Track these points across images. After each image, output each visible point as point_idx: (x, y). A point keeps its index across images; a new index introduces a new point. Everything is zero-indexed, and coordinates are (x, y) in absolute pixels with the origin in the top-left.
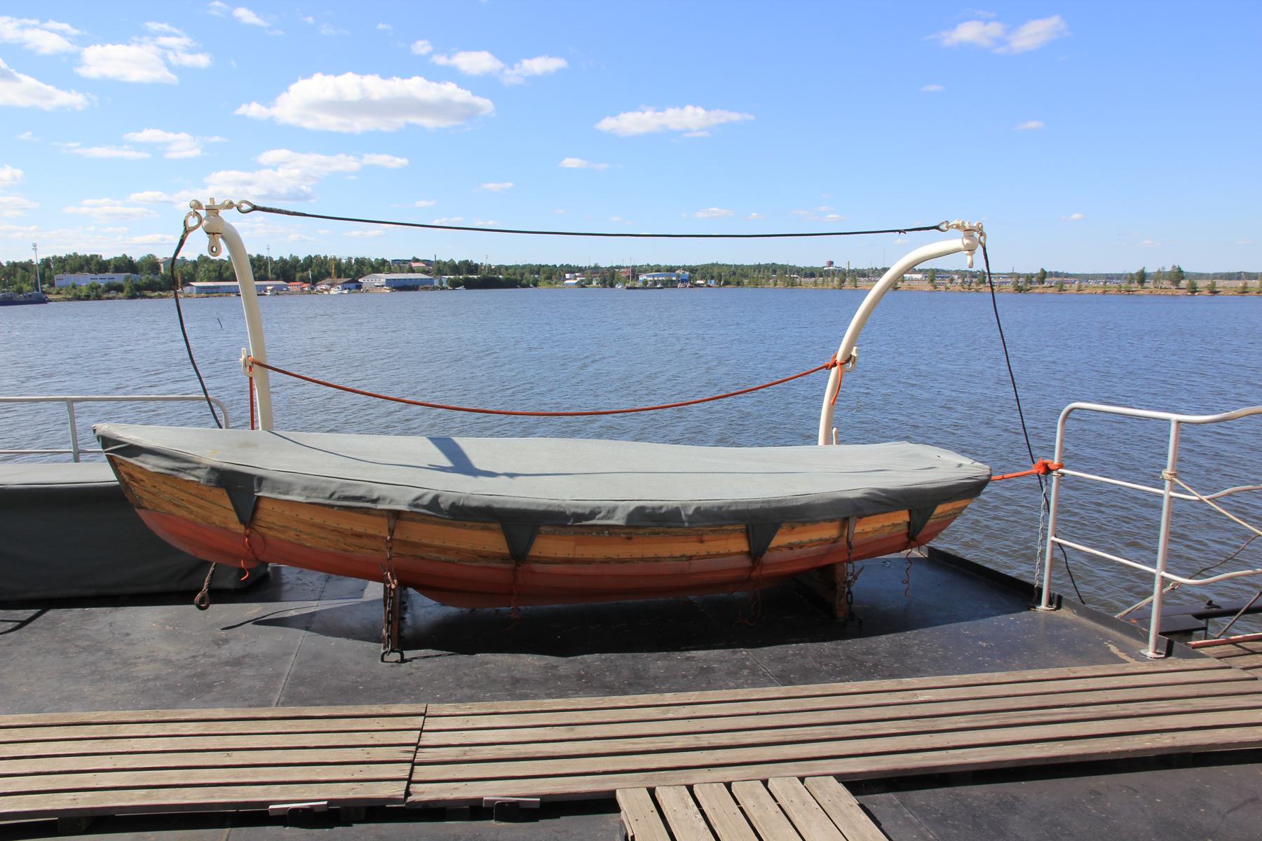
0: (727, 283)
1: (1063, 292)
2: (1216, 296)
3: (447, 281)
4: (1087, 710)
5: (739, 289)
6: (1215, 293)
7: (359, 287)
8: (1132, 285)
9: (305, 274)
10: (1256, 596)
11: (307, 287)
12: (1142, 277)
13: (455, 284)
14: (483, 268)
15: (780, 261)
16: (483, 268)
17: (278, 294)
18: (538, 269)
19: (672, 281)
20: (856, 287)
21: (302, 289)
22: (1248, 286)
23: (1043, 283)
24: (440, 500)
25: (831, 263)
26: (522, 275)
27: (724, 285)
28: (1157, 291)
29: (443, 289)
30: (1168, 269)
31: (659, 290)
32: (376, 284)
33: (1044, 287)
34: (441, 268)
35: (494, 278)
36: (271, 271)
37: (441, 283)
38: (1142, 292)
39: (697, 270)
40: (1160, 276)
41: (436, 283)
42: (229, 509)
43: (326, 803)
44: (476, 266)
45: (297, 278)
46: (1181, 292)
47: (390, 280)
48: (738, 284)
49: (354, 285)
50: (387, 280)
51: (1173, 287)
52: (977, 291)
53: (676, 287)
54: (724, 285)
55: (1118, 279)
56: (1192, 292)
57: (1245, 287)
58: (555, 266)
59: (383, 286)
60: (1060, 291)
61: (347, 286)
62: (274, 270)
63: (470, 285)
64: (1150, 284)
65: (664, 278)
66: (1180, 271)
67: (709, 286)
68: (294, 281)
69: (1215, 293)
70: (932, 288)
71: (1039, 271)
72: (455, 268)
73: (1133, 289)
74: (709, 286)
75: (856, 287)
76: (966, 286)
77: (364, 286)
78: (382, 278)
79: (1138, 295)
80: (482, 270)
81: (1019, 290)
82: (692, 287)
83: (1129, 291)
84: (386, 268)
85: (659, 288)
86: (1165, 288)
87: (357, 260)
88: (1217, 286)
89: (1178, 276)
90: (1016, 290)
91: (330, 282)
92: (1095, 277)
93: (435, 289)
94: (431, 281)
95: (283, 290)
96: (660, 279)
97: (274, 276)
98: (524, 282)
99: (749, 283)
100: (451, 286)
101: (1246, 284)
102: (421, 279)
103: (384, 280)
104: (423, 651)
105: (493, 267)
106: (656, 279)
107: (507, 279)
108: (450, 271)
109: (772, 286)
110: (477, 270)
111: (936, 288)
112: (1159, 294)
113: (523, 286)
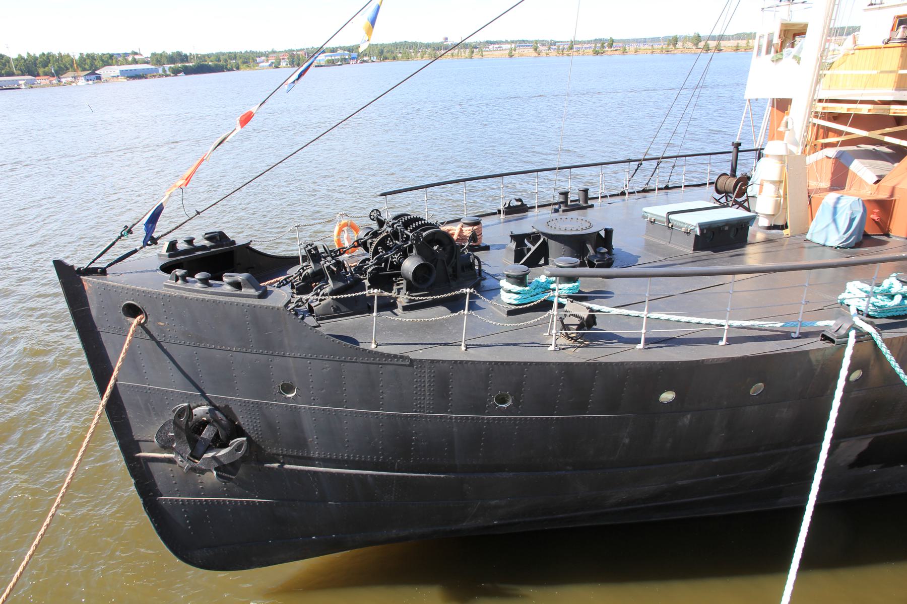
0: (386, 58)
1: (626, 54)
2: (721, 53)
3: (169, 70)
4: (713, 291)
5: (395, 62)
6: (720, 50)
7: (99, 78)
8: (670, 47)
9: (46, 69)
10: (5, 354)
11: (55, 81)
12: (675, 41)
13: (176, 72)
14: (192, 57)
15: (410, 39)
16: (192, 57)
17: (32, 88)
18: (234, 56)
19: (345, 59)
20: (482, 56)
21: (50, 81)
22: (739, 45)
23: (611, 47)
24: (194, 241)
25: (446, 39)
26: (226, 61)
27: (383, 60)
28: (685, 51)
29: (167, 76)
30: (692, 34)
31: (339, 66)
32: (112, 75)
33: (611, 51)
34: (159, 59)
35: (205, 65)
36: (16, 67)
37: (164, 71)
38: (676, 52)
39: (353, 50)
40: (686, 39)
41: (161, 71)
42: (93, 262)
43: (891, 276)
44: (186, 56)
45: (41, 74)
46: (699, 51)
47: (123, 71)
48: (394, 58)
49: (94, 76)
50: (121, 71)
51: (694, 47)
52: (568, 55)
53: (349, 63)
54: (383, 60)
55: (651, 42)
56: (706, 50)
57: (738, 46)
58: (241, 52)
59: (118, 76)
60: (623, 53)
61: (89, 77)
62: (18, 67)
63: (188, 71)
64: (679, 45)
65: (339, 57)
66: (699, 36)
67: (373, 62)
68: (38, 75)
69: (720, 50)
70: (537, 55)
71: (609, 38)
72: (172, 59)
73: (670, 50)
74: (373, 62)
75: (482, 56)
76: (560, 52)
77: (102, 76)
78: (115, 70)
79: (674, 54)
80: (191, 59)
81: (596, 53)
82: (362, 63)
83: (668, 51)
84: (114, 61)
85: (339, 65)
86: (689, 48)
87: (88, 55)
88: (722, 45)
89: (697, 39)
90: (595, 53)
91: (73, 75)
92: (645, 41)
93: (161, 76)
94: (156, 70)
95: (34, 84)
96: (336, 58)
97: (20, 72)
98: (229, 67)
99: (402, 57)
100: (173, 73)
101: (738, 44)
102: (148, 69)
103: (119, 72)
104: (706, 252)
105: (199, 56)
106: (333, 58)
107: (216, 65)
108: (167, 61)
109: (420, 58)
110: (187, 59)
111: (539, 54)
112: (687, 53)
113: (229, 70)
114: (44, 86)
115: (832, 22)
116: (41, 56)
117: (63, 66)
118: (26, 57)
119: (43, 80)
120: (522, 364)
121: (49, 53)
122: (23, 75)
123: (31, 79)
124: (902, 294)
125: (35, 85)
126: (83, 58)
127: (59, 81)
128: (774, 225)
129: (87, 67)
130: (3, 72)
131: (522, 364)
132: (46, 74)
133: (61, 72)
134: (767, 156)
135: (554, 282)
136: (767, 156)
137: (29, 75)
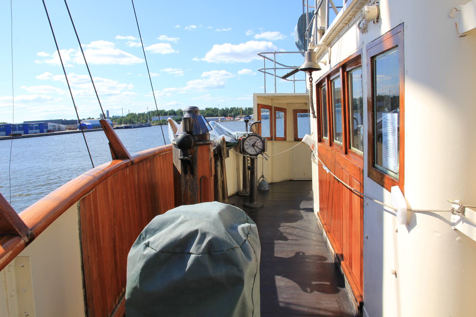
9: (231, 114)
17: (222, 121)
21: (230, 119)
36: (220, 113)
45: (228, 116)
77: (252, 118)
87: (249, 108)
97: (221, 115)
114: (227, 121)
115: (306, 8)
116: (230, 109)
117: (237, 113)
118: (225, 109)
119: (227, 119)
120: (276, 239)
121: (234, 107)
122: (221, 116)
123: (223, 118)
124: (354, 136)
125: (224, 121)
126: (247, 109)
127: (234, 119)
128: (126, 116)
129: (247, 113)
130: (215, 115)
131: (276, 239)
132: (230, 116)
133: (236, 115)
134: (407, 204)
135: (122, 293)
136: (407, 204)
137: (224, 116)
